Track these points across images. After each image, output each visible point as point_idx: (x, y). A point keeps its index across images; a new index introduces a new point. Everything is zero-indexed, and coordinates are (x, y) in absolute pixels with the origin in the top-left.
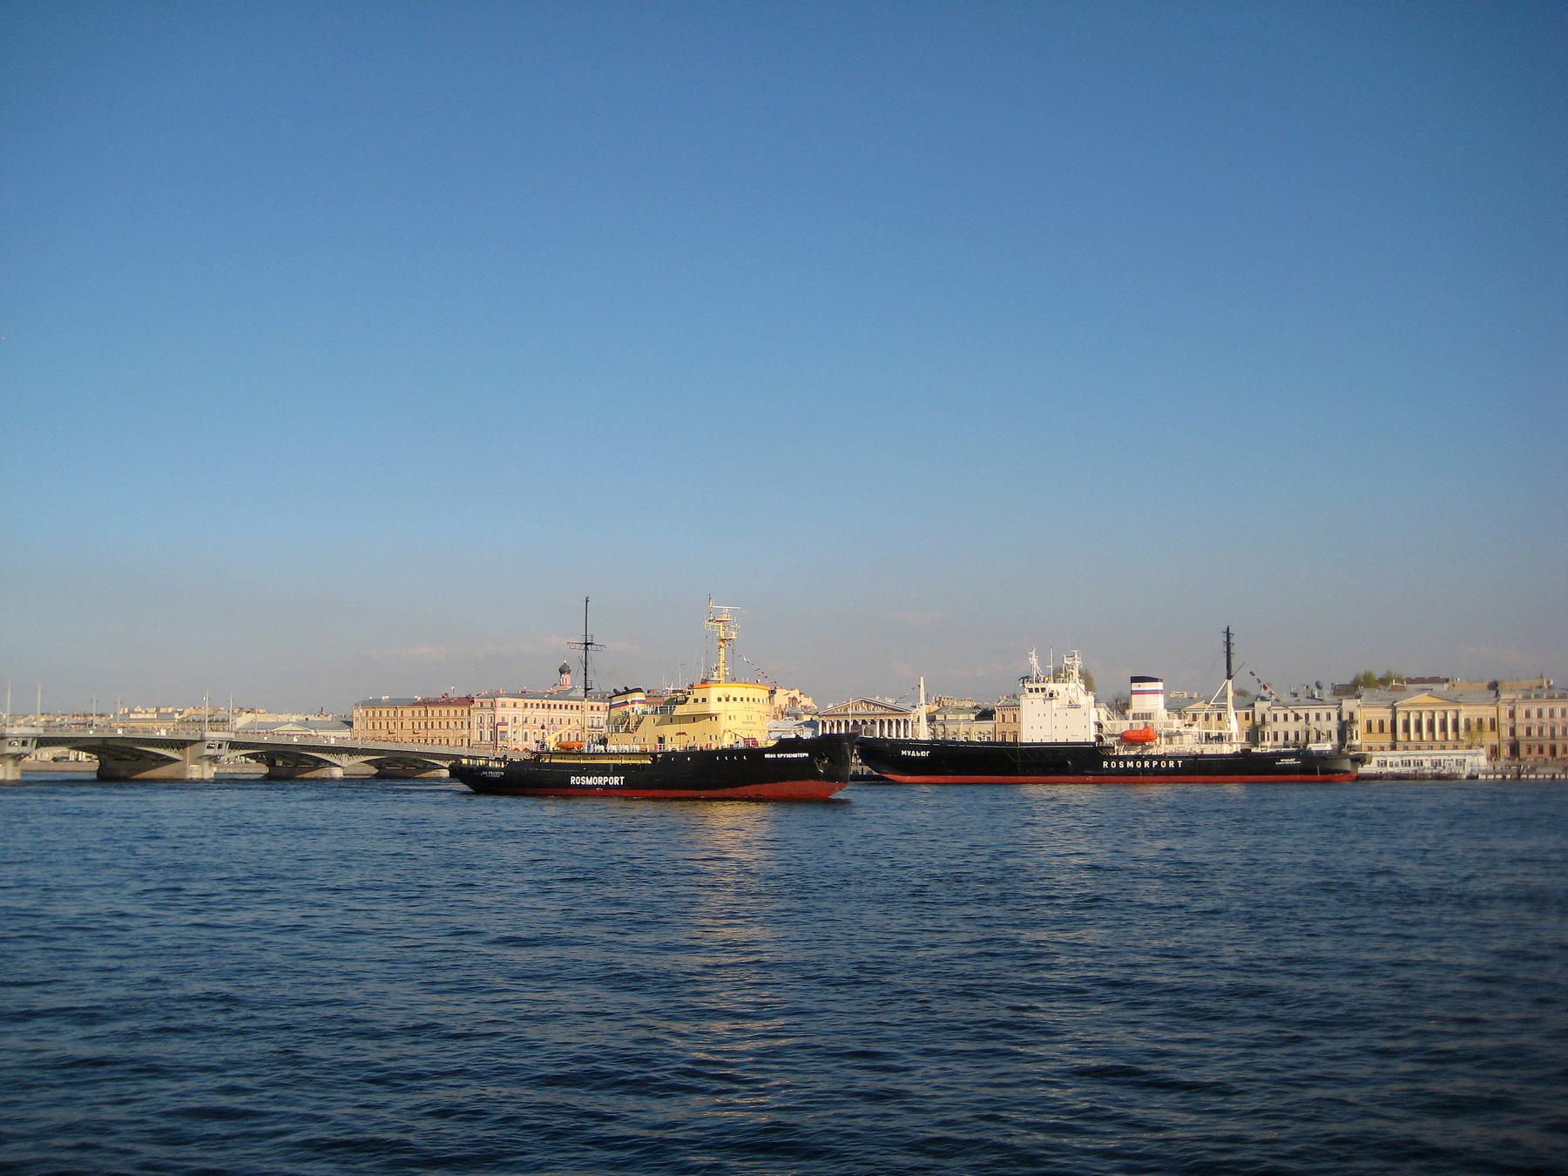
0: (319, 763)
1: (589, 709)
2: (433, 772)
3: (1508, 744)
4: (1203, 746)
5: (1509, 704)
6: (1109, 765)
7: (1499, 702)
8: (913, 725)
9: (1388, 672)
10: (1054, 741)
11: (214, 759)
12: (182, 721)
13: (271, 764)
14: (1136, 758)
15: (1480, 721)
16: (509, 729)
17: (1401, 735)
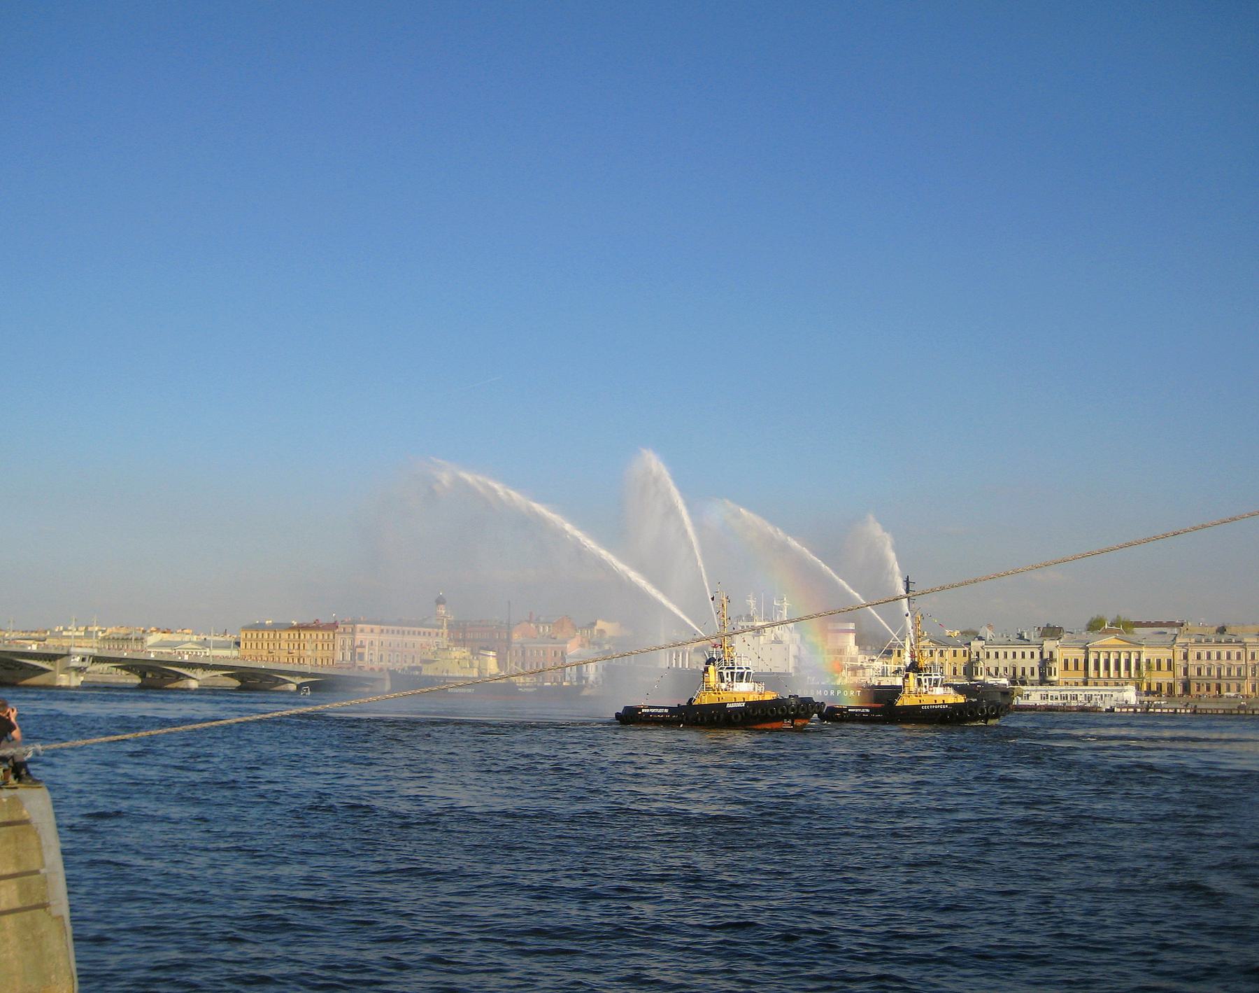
0: (179, 676)
1: (435, 635)
2: (283, 686)
3: (1181, 682)
4: (880, 678)
5: (1183, 647)
7: (1175, 646)
9: (1118, 616)
11: (79, 670)
12: (104, 639)
13: (143, 676)
15: (1159, 662)
16: (366, 651)
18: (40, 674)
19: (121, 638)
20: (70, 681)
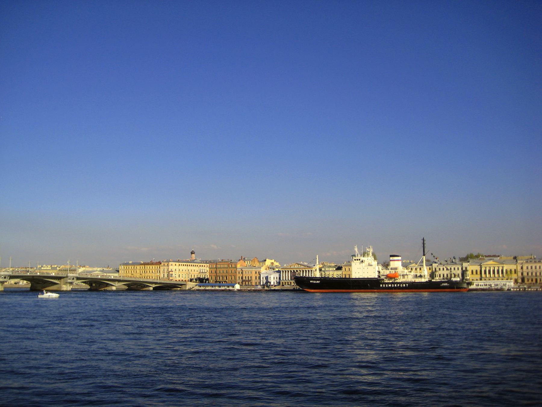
0: (108, 285)
1: (199, 266)
5: (521, 264)
6: (383, 286)
7: (517, 264)
10: (363, 277)
11: (71, 283)
12: (60, 270)
13: (91, 285)
14: (392, 283)
16: (173, 273)
18: (54, 285)
19: (73, 269)
20: (67, 288)
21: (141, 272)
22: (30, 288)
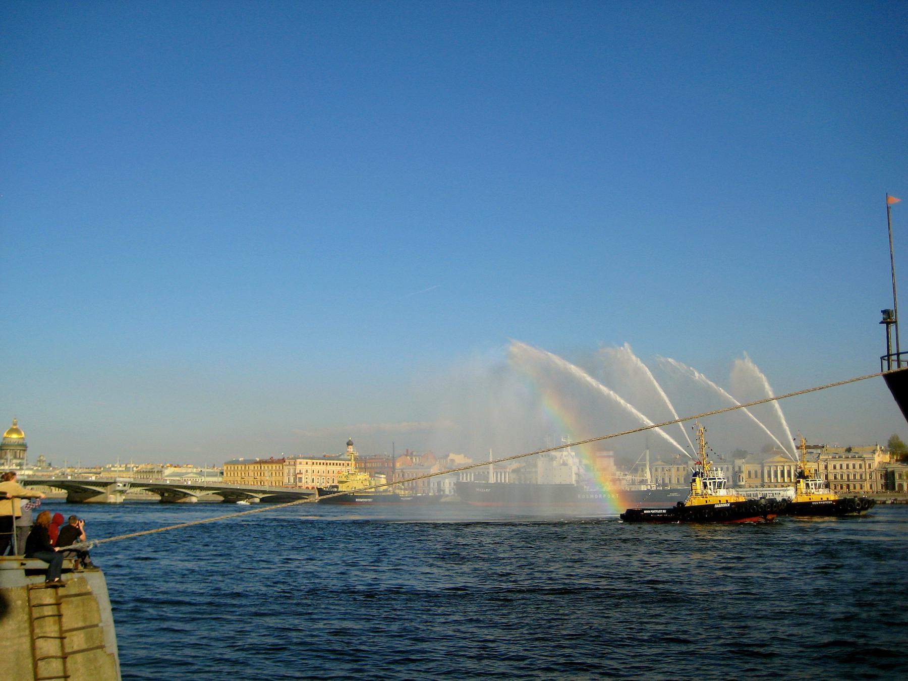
0: (185, 495)
1: (347, 465)
8: (508, 474)
12: (137, 472)
13: (162, 495)
16: (303, 476)
17: (766, 479)
21: (256, 475)
22: (65, 499)
